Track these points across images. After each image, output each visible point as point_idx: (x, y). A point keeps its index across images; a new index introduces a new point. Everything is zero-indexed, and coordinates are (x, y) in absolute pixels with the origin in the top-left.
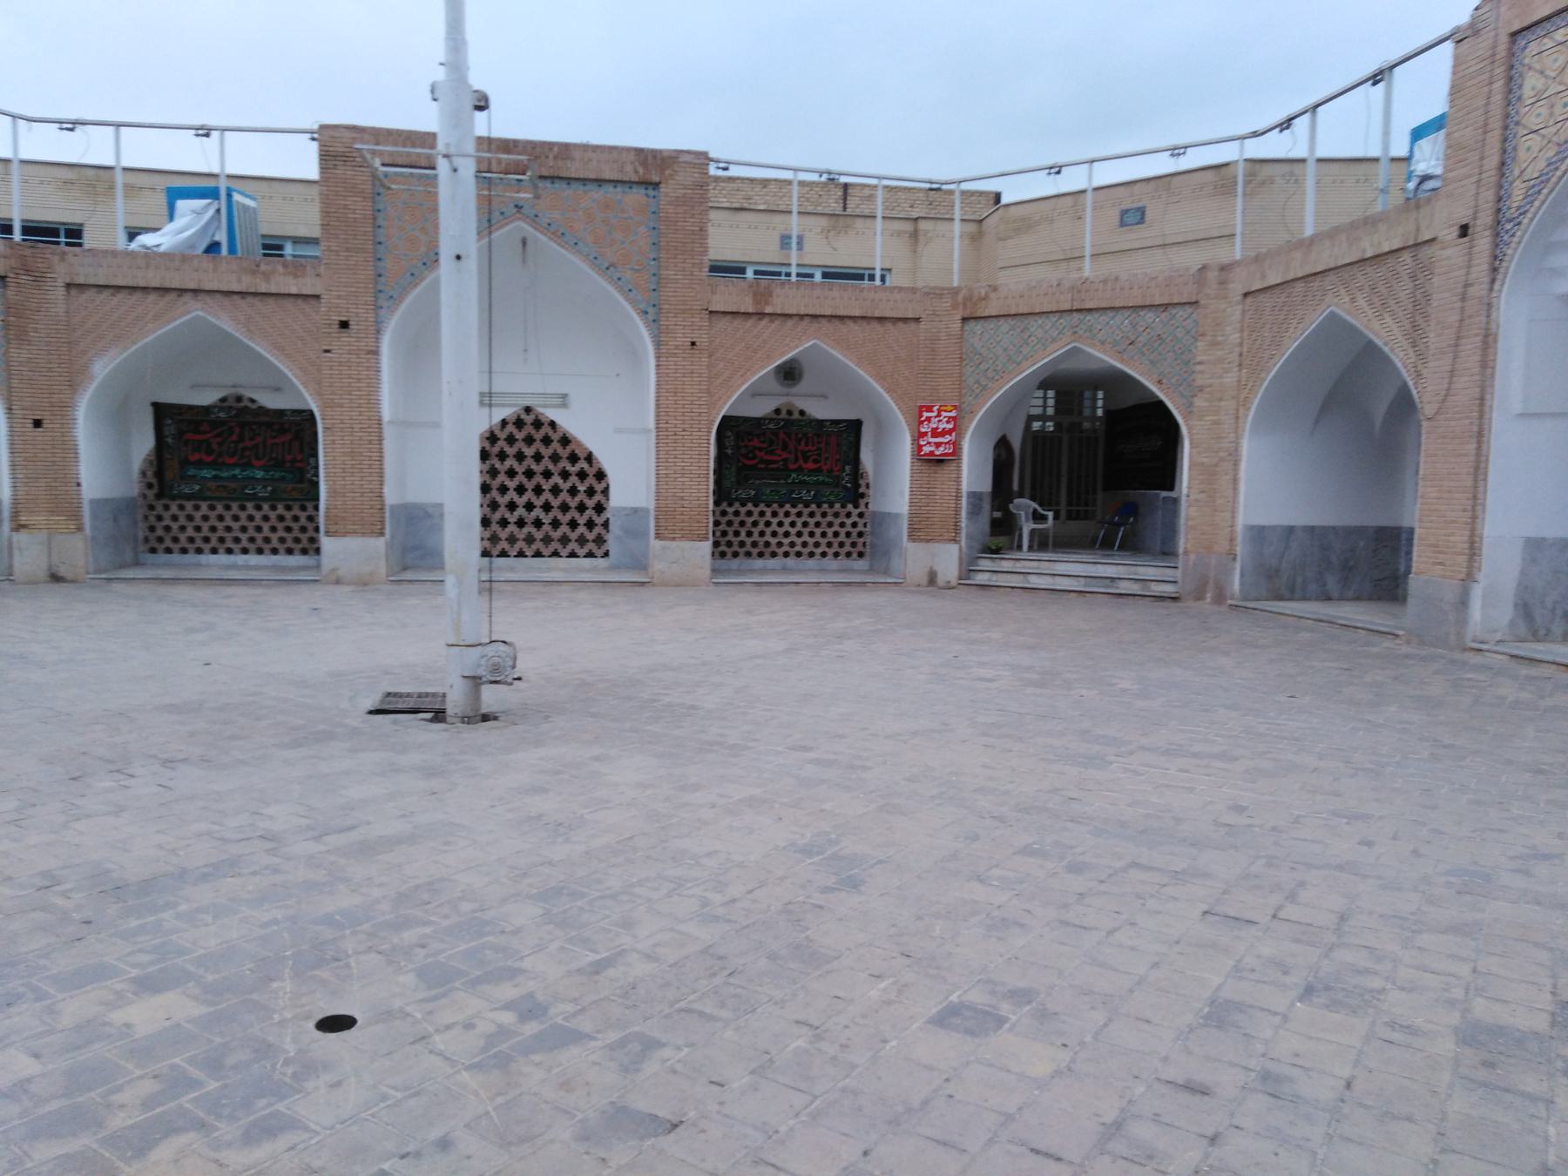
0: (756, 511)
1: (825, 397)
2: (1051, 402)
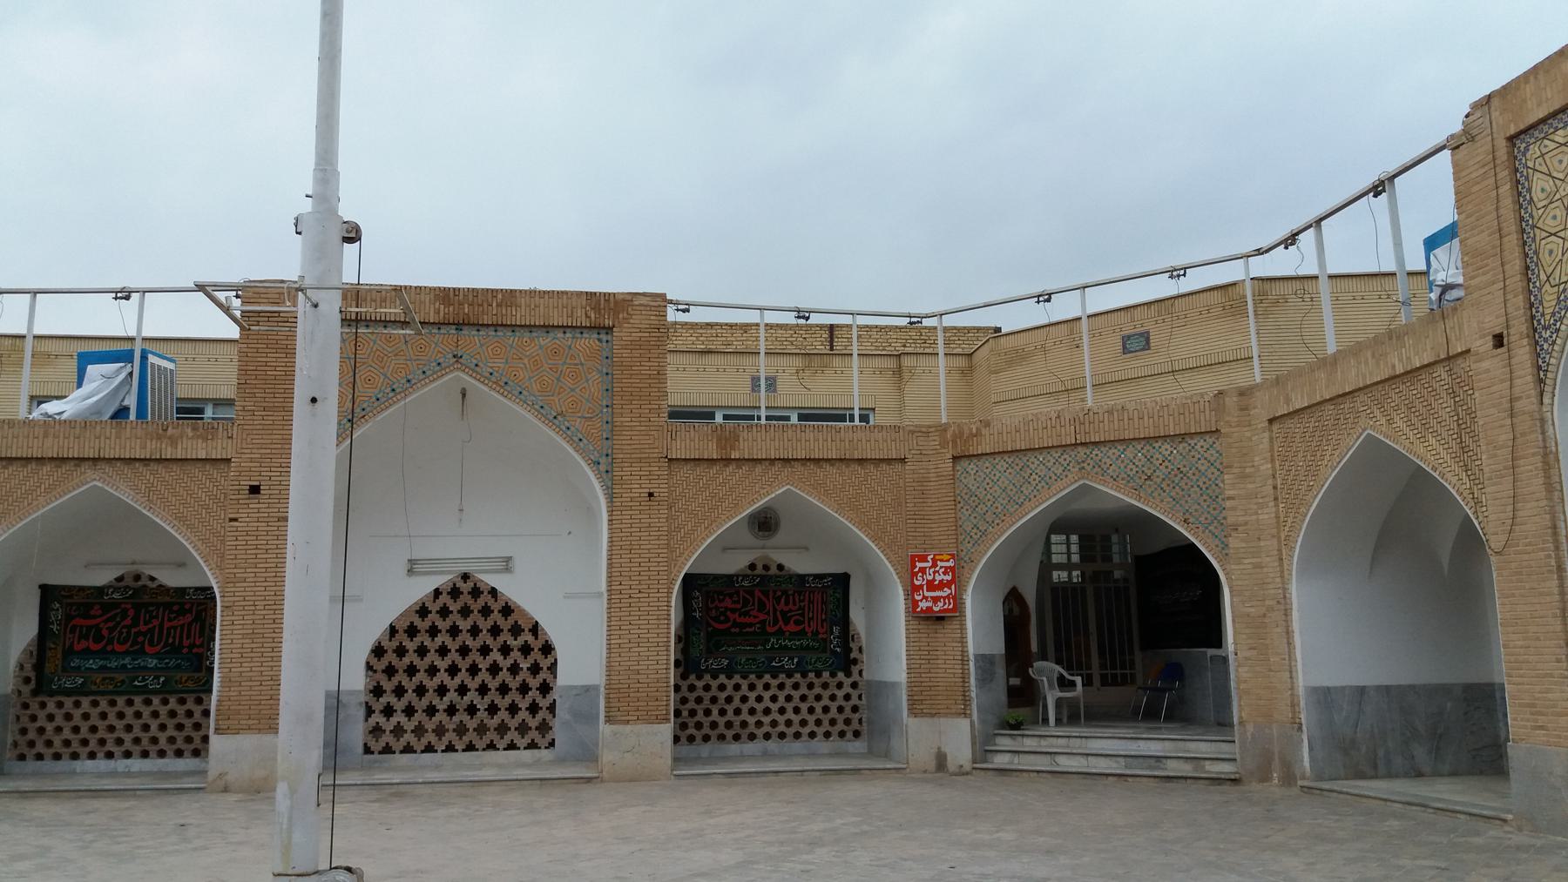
0: (730, 684)
1: (806, 548)
2: (1074, 548)
